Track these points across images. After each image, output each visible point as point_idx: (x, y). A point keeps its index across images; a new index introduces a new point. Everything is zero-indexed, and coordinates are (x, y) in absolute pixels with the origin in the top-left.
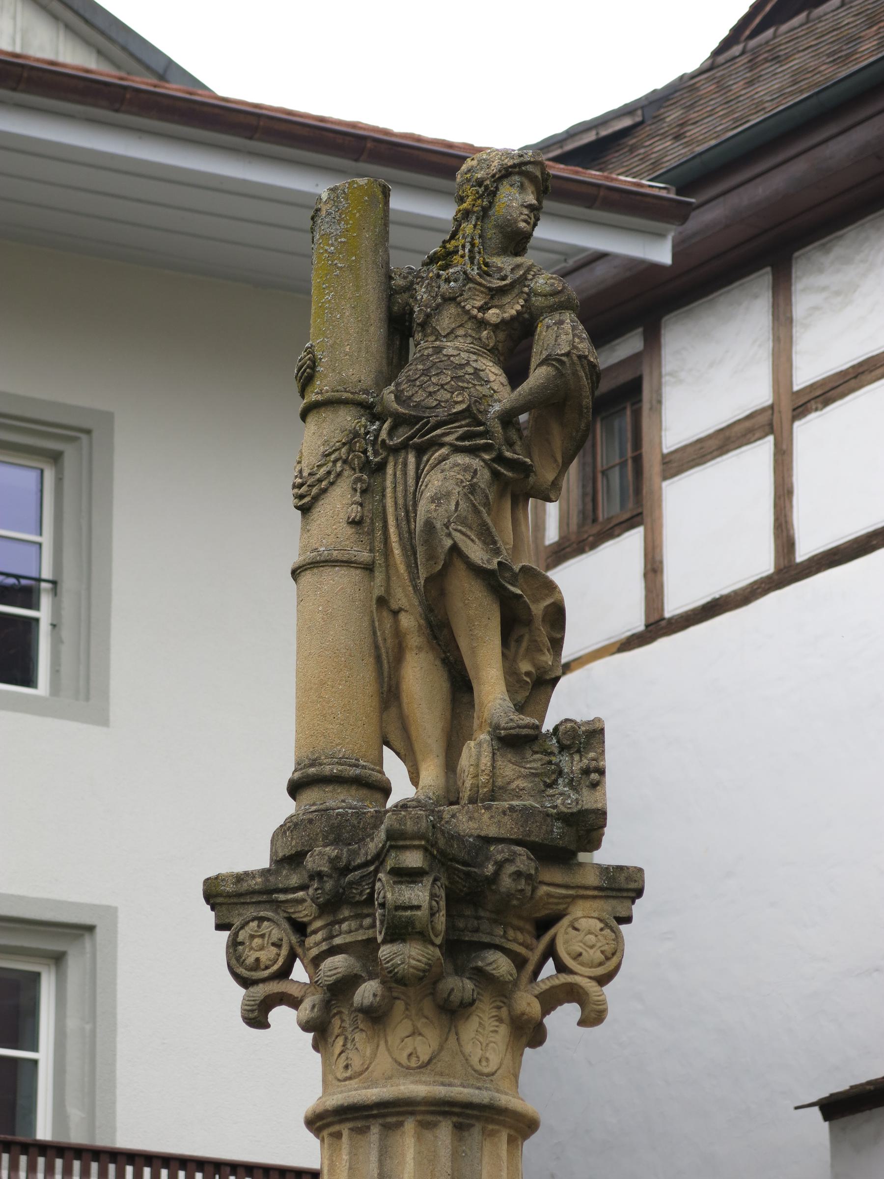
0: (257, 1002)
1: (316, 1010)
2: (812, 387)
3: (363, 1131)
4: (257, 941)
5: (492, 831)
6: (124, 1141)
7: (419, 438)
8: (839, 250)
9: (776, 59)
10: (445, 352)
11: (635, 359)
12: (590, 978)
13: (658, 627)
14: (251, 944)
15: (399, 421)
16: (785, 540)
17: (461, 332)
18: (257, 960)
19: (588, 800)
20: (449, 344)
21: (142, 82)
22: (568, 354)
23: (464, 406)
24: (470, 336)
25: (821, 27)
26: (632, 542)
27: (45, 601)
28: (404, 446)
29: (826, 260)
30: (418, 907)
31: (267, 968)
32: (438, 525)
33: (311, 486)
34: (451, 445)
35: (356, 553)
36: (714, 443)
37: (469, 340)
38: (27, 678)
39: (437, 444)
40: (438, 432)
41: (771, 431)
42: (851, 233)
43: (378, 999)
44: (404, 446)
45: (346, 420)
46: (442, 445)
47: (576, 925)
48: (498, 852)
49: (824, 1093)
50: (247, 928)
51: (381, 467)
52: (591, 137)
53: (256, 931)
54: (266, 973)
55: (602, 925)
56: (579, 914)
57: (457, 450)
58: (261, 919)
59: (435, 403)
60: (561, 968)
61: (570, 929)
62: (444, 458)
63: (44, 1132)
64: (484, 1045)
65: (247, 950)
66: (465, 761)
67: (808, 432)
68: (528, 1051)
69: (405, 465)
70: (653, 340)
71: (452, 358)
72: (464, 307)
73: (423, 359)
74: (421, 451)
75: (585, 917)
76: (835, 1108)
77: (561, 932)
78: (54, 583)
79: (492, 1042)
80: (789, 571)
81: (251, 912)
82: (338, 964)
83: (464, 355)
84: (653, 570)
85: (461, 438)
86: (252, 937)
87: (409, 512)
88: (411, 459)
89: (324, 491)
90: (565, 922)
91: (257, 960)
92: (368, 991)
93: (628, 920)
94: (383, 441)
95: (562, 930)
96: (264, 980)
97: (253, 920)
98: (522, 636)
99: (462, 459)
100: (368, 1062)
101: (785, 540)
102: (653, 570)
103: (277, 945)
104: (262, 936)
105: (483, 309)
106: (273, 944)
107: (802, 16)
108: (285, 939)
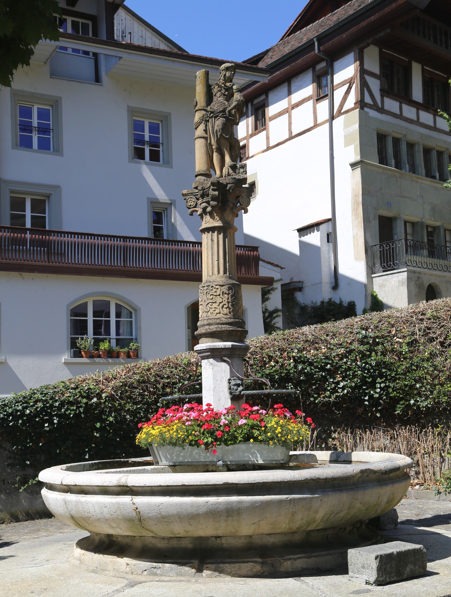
2: (295, 104)
3: (209, 233)
5: (228, 182)
6: (64, 230)
8: (299, 79)
9: (288, 43)
11: (264, 100)
13: (269, 148)
15: (212, 112)
16: (290, 132)
19: (245, 176)
21: (175, 50)
25: (297, 36)
26: (265, 132)
27: (161, 147)
28: (212, 117)
29: (297, 80)
36: (278, 115)
38: (158, 161)
39: (218, 116)
41: (288, 112)
42: (301, 75)
44: (212, 117)
45: (203, 112)
48: (229, 186)
49: (298, 228)
51: (208, 121)
52: (255, 59)
57: (221, 117)
60: (240, 204)
62: (219, 118)
63: (165, 238)
66: (224, 170)
67: (294, 112)
70: (267, 96)
73: (215, 101)
76: (328, 241)
77: (240, 198)
78: (162, 144)
80: (291, 138)
81: (189, 197)
82: (204, 205)
84: (268, 138)
87: (213, 128)
88: (213, 119)
89: (199, 125)
92: (209, 209)
96: (192, 208)
99: (221, 119)
101: (290, 132)
102: (268, 138)
103: (194, 202)
105: (225, 92)
107: (299, 32)
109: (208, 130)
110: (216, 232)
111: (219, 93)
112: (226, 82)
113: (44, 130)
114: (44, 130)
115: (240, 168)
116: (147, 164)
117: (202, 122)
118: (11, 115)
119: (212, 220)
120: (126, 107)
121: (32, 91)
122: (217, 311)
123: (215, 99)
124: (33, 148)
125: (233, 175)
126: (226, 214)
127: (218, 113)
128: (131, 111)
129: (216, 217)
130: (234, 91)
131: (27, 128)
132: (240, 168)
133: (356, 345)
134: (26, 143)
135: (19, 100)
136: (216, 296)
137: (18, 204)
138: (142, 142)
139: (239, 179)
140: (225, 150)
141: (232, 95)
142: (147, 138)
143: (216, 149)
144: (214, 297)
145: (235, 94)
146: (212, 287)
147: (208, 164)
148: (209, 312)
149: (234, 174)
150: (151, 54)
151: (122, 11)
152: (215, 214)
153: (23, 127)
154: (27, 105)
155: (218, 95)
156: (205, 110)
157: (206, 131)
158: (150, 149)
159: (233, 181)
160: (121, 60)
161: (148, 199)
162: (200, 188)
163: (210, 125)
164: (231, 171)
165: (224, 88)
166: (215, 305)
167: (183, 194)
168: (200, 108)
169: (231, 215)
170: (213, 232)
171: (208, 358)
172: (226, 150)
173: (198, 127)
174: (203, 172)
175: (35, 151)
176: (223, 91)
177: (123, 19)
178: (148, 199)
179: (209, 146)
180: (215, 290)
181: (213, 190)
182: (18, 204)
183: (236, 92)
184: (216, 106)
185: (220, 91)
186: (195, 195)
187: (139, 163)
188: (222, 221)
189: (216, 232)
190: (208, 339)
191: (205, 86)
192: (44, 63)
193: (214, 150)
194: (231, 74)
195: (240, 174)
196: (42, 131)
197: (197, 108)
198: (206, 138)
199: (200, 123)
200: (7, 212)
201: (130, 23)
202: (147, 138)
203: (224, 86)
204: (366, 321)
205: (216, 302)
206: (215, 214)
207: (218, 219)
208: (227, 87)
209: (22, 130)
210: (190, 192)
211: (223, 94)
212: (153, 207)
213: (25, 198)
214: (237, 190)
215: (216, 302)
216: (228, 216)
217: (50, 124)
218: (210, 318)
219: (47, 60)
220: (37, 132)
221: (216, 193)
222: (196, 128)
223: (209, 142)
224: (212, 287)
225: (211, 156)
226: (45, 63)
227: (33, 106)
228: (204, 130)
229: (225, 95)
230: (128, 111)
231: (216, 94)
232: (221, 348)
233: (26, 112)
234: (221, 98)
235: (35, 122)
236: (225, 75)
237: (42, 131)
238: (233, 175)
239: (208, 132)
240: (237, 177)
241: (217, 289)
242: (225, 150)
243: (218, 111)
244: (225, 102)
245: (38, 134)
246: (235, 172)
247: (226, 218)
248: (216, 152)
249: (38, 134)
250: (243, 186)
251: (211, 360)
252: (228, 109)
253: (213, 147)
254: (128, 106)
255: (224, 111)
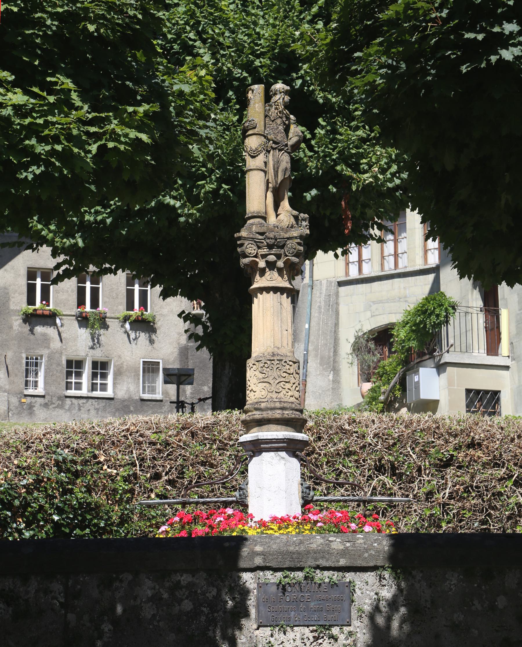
28: (275, 149)
44: (275, 149)
110: (285, 294)
119: (280, 278)
122: (290, 393)
129: (285, 276)
133: (51, 472)
136: (289, 374)
144: (287, 375)
146: (286, 362)
148: (282, 393)
166: (288, 386)
170: (282, 294)
171: (277, 451)
180: (288, 367)
185: (281, 118)
186: (255, 242)
189: (285, 294)
190: (279, 427)
198: (265, 172)
204: (44, 441)
205: (289, 382)
210: (251, 236)
215: (289, 382)
218: (282, 400)
221: (302, 248)
224: (286, 362)
232: (297, 440)
241: (291, 366)
251: (283, 454)
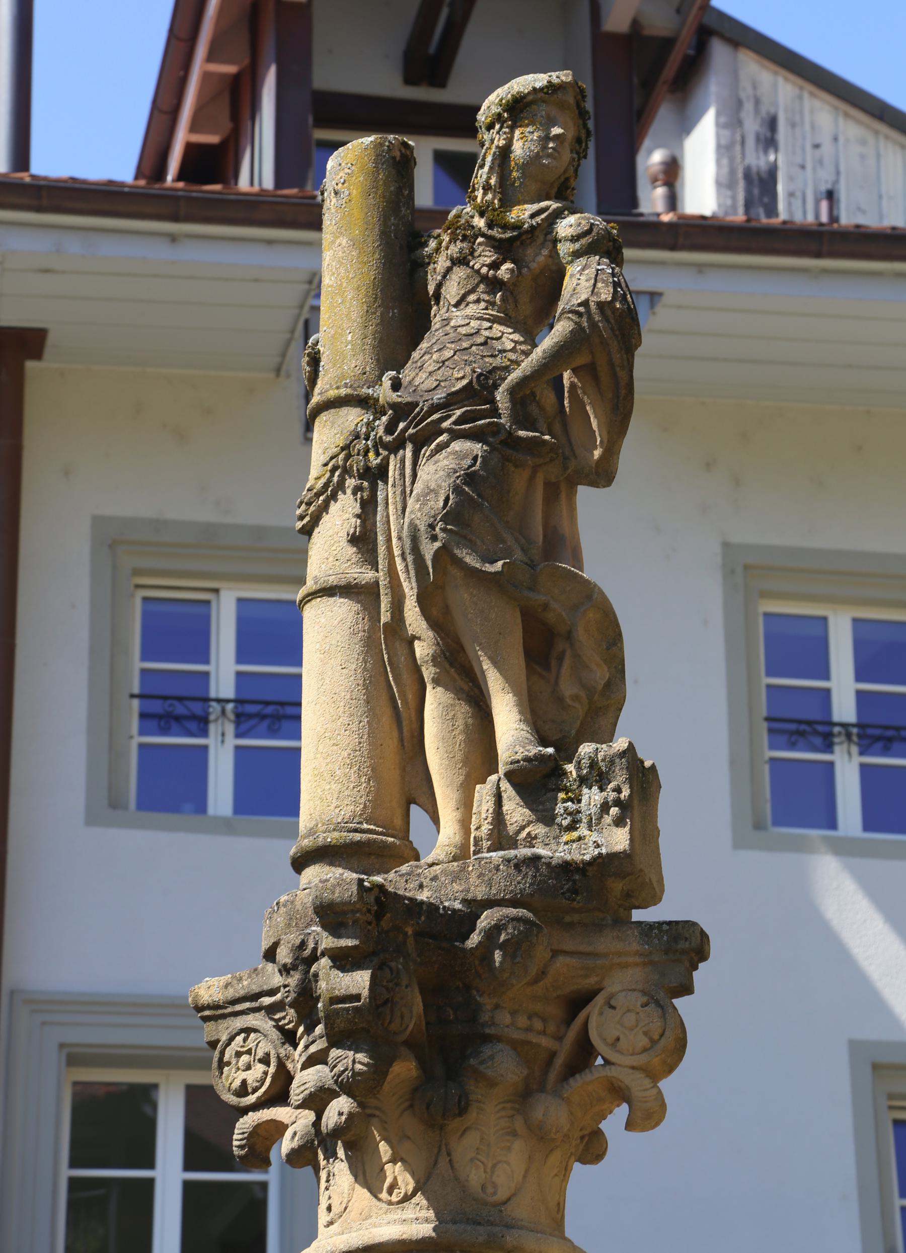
0: (246, 1135)
1: (296, 1138)
4: (245, 1058)
5: (480, 892)
7: (414, 428)
10: (452, 323)
12: (633, 1068)
14: (238, 1062)
15: (402, 411)
17: (472, 297)
18: (244, 1082)
20: (458, 313)
22: (585, 303)
23: (465, 382)
24: (484, 300)
30: (357, 997)
31: (255, 1090)
32: (422, 528)
33: (309, 504)
34: (448, 430)
35: (356, 576)
37: (483, 305)
40: (436, 416)
43: (344, 1118)
44: (396, 447)
46: (441, 433)
47: (613, 1002)
48: (486, 920)
50: (233, 1043)
51: (382, 472)
53: (242, 1047)
54: (251, 1099)
55: (645, 999)
56: (616, 988)
57: (456, 435)
58: (248, 1031)
59: (435, 384)
61: (606, 1008)
62: (446, 445)
64: (490, 1165)
65: (234, 1070)
68: (578, 1168)
69: (403, 461)
71: (459, 329)
72: (473, 267)
74: (420, 442)
75: (624, 990)
79: (500, 1162)
83: (474, 324)
85: (460, 421)
86: (238, 1054)
89: (325, 507)
90: (600, 999)
91: (244, 1082)
93: (686, 989)
94: (381, 437)
95: (596, 1011)
96: (255, 1107)
97: (238, 1034)
98: (563, 653)
100: (345, 1201)
103: (265, 1061)
104: (249, 1052)
105: (495, 266)
106: (260, 1061)
108: (273, 1053)
109: (381, 539)
111: (460, 273)
112: (507, 203)
113: (269, 710)
114: (269, 710)
115: (583, 781)
116: (844, 849)
117: (341, 486)
118: (93, 651)
120: (718, 550)
121: (205, 514)
123: (438, 315)
124: (211, 810)
125: (531, 840)
126: (472, 1139)
127: (434, 409)
128: (746, 567)
129: (395, 1172)
130: (564, 249)
131: (179, 709)
132: (583, 781)
134: (171, 789)
135: (137, 572)
137: (112, 1124)
138: (816, 733)
139: (567, 867)
140: (486, 665)
141: (555, 278)
142: (844, 708)
143: (434, 659)
145: (573, 270)
147: (375, 774)
149: (539, 829)
150: (818, 255)
151: (817, 104)
152: (384, 1149)
153: (157, 707)
154: (186, 591)
155: (452, 291)
156: (364, 402)
157: (363, 540)
158: (863, 767)
159: (523, 883)
160: (659, 309)
161: (856, 1047)
162: (284, 955)
163: (388, 492)
164: (516, 812)
165: (492, 242)
167: (199, 1008)
168: (332, 393)
169: (518, 1145)
172: (495, 663)
173: (316, 520)
174: (332, 837)
175: (224, 827)
176: (485, 257)
177: (826, 141)
178: (856, 1047)
179: (383, 645)
181: (344, 961)
182: (112, 1124)
183: (577, 255)
184: (431, 371)
185: (461, 261)
187: (801, 846)
188: (433, 1203)
191: (373, 241)
192: (272, 375)
193: (428, 673)
194: (547, 138)
195: (583, 830)
196: (263, 717)
197: (315, 399)
199: (330, 493)
200: (48, 1168)
201: (862, 157)
202: (844, 708)
203: (490, 226)
206: (384, 1149)
207: (407, 1183)
208: (505, 227)
209: (154, 720)
210: (240, 990)
211: (484, 279)
212: (891, 1096)
213: (155, 1086)
214: (555, 953)
216: (495, 1158)
217: (144, 658)
219: (283, 355)
220: (230, 728)
221: (359, 981)
222: (308, 531)
223: (385, 617)
225: (408, 716)
226: (278, 371)
227: (216, 591)
228: (353, 540)
229: (494, 284)
230: (729, 572)
231: (439, 286)
233: (178, 630)
234: (472, 310)
235: (224, 672)
236: (505, 152)
237: (263, 717)
238: (531, 840)
239: (382, 549)
240: (557, 850)
242: (486, 665)
243: (439, 396)
244: (498, 329)
245: (238, 735)
246: (548, 819)
247: (475, 1177)
248: (437, 682)
249: (238, 735)
250: (637, 915)
252: (514, 376)
253: (422, 650)
254: (726, 545)
255: (479, 391)
